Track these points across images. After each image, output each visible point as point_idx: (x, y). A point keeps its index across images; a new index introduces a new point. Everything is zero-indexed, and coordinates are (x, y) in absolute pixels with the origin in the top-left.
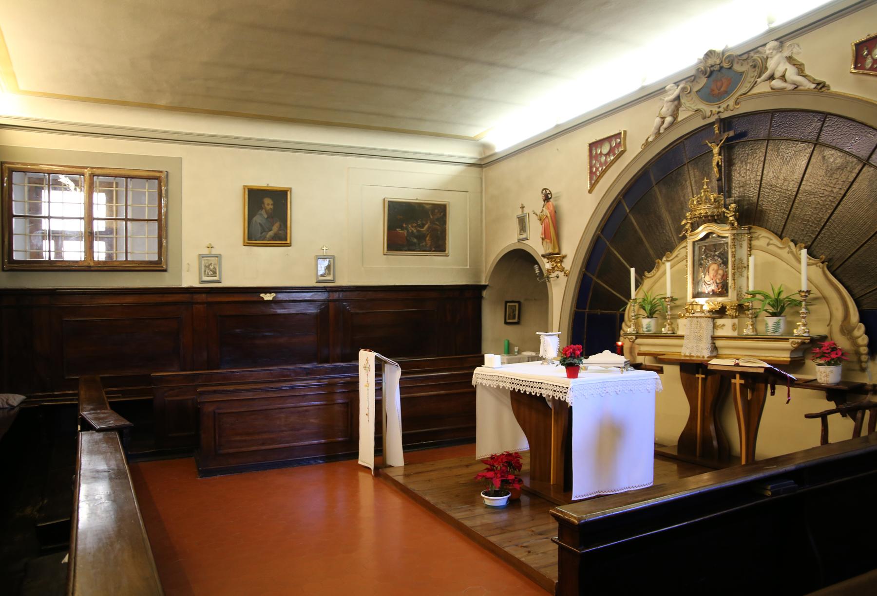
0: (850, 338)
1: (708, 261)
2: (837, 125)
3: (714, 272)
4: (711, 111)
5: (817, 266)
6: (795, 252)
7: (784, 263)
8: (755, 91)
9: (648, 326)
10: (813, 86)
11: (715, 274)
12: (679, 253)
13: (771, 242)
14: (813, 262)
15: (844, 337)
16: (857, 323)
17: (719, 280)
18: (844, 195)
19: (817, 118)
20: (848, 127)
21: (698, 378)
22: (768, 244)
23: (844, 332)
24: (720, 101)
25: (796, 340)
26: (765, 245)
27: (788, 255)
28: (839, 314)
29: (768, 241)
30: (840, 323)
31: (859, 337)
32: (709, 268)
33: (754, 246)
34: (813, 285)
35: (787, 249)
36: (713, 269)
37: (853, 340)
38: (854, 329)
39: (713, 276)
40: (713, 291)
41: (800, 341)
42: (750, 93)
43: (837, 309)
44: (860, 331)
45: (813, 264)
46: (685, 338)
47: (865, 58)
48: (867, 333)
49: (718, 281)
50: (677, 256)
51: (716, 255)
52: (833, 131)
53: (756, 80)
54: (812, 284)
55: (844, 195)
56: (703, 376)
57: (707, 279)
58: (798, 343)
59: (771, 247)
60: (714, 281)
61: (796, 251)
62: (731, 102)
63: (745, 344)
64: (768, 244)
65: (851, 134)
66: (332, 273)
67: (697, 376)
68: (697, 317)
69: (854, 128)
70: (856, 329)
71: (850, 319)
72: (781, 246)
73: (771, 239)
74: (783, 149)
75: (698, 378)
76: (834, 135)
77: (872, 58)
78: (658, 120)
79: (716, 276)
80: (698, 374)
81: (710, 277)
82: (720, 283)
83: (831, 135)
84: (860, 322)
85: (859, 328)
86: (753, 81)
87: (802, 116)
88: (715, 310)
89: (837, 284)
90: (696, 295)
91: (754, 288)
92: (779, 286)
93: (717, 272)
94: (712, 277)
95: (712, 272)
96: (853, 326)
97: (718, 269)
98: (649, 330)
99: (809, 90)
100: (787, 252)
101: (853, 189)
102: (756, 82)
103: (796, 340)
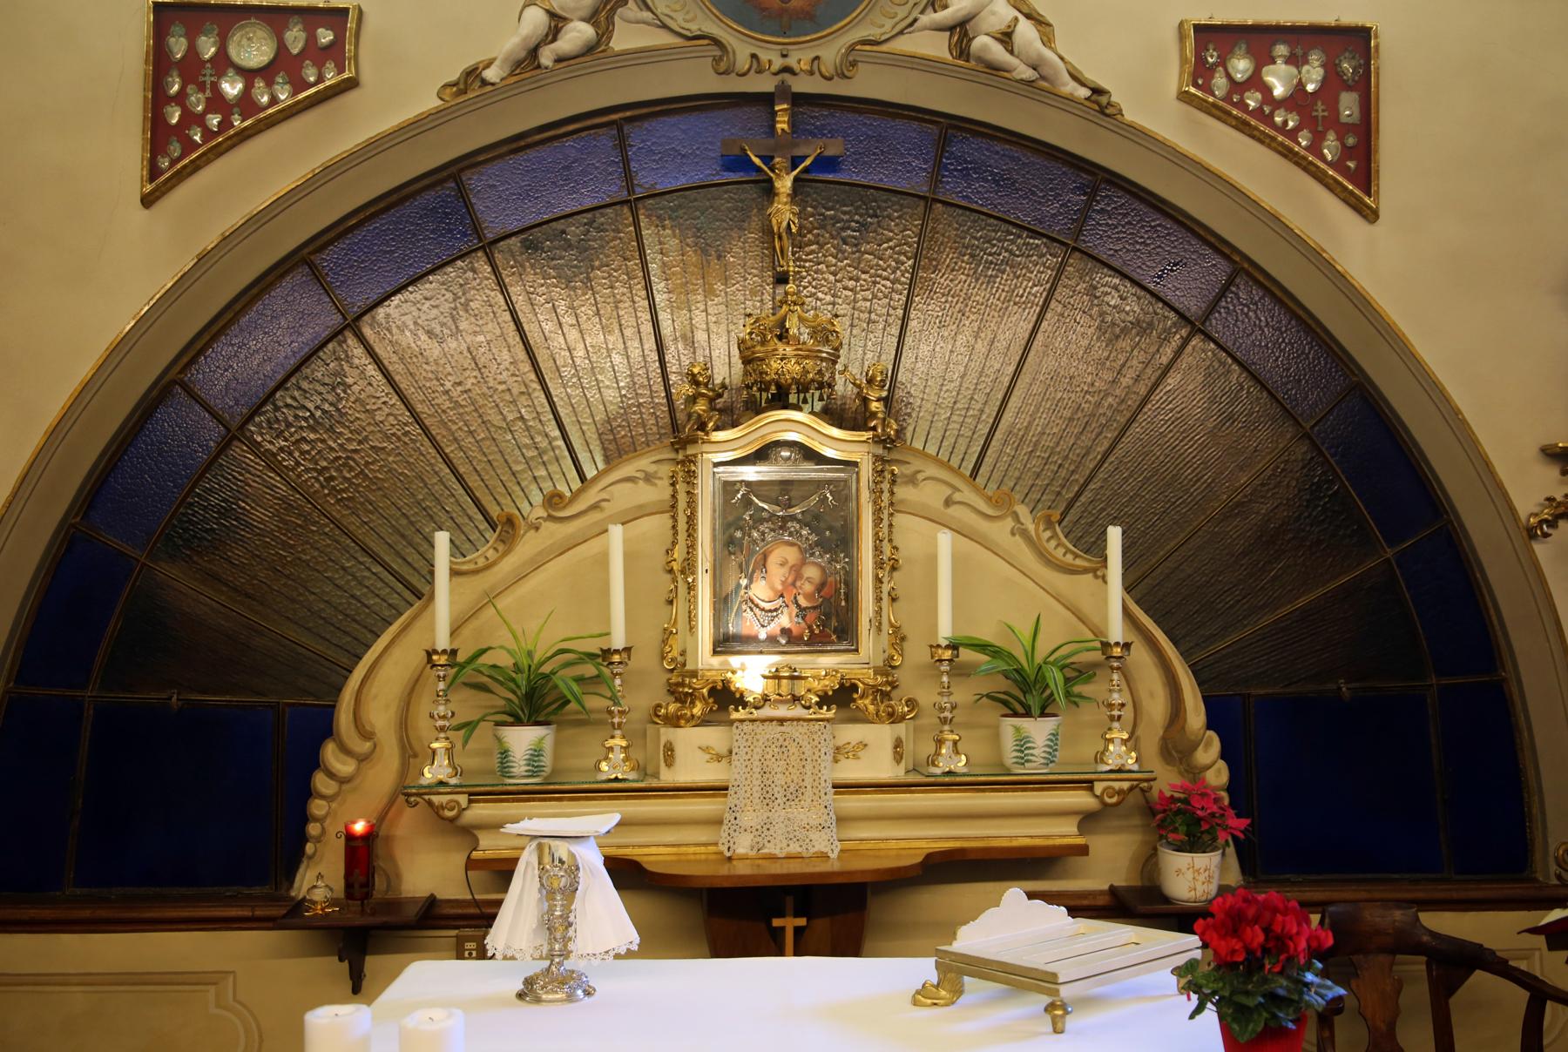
0: (1186, 771)
1: (763, 533)
2: (1125, 215)
3: (785, 570)
4: (754, 56)
5: (1096, 577)
6: (1033, 533)
7: (1001, 560)
8: (904, 45)
9: (536, 754)
10: (1083, 93)
11: (790, 580)
12: (604, 495)
13: (957, 497)
14: (1086, 564)
15: (1170, 768)
16: (1202, 731)
17: (807, 596)
18: (1145, 401)
19: (1074, 182)
20: (1152, 227)
21: (783, 929)
22: (948, 502)
23: (1170, 754)
24: (784, 34)
25: (1117, 785)
26: (937, 503)
27: (1013, 539)
28: (1156, 707)
29: (948, 491)
30: (1161, 733)
31: (1208, 767)
32: (765, 557)
33: (902, 501)
34: (1087, 626)
35: (1009, 523)
36: (779, 560)
37: (1195, 773)
38: (1195, 746)
39: (783, 583)
40: (785, 631)
41: (1126, 785)
42: (884, 48)
43: (1152, 695)
44: (1209, 752)
45: (1085, 571)
46: (730, 792)
47: (1211, 70)
48: (1224, 755)
49: (803, 602)
50: (595, 507)
51: (793, 518)
52: (1116, 227)
53: (915, 14)
54: (1084, 623)
55: (1145, 401)
56: (802, 922)
57: (760, 590)
58: (1120, 792)
59: (954, 511)
60: (788, 598)
61: (1037, 530)
62: (831, 52)
63: (938, 803)
64: (948, 502)
65: (1160, 247)
66: (1097, 171)
67: (776, 922)
68: (781, 721)
69: (1168, 234)
70: (1201, 748)
71: (1185, 720)
72: (990, 512)
73: (957, 489)
74: (975, 238)
75: (783, 929)
76: (1119, 239)
77: (1229, 76)
78: (535, 19)
79: (794, 584)
80: (782, 915)
81: (772, 588)
82: (814, 608)
83: (1110, 237)
84: (1209, 727)
85: (1209, 744)
86: (901, 14)
87: (1034, 163)
88: (834, 691)
89: (1150, 628)
90: (725, 643)
91: (953, 633)
92: (485, 647)
93: (797, 571)
94: (780, 587)
95: (777, 574)
96: (1193, 738)
97: (803, 563)
98: (534, 770)
99: (1070, 99)
100: (1009, 529)
101: (1168, 388)
102: (915, 20)
103: (1117, 785)
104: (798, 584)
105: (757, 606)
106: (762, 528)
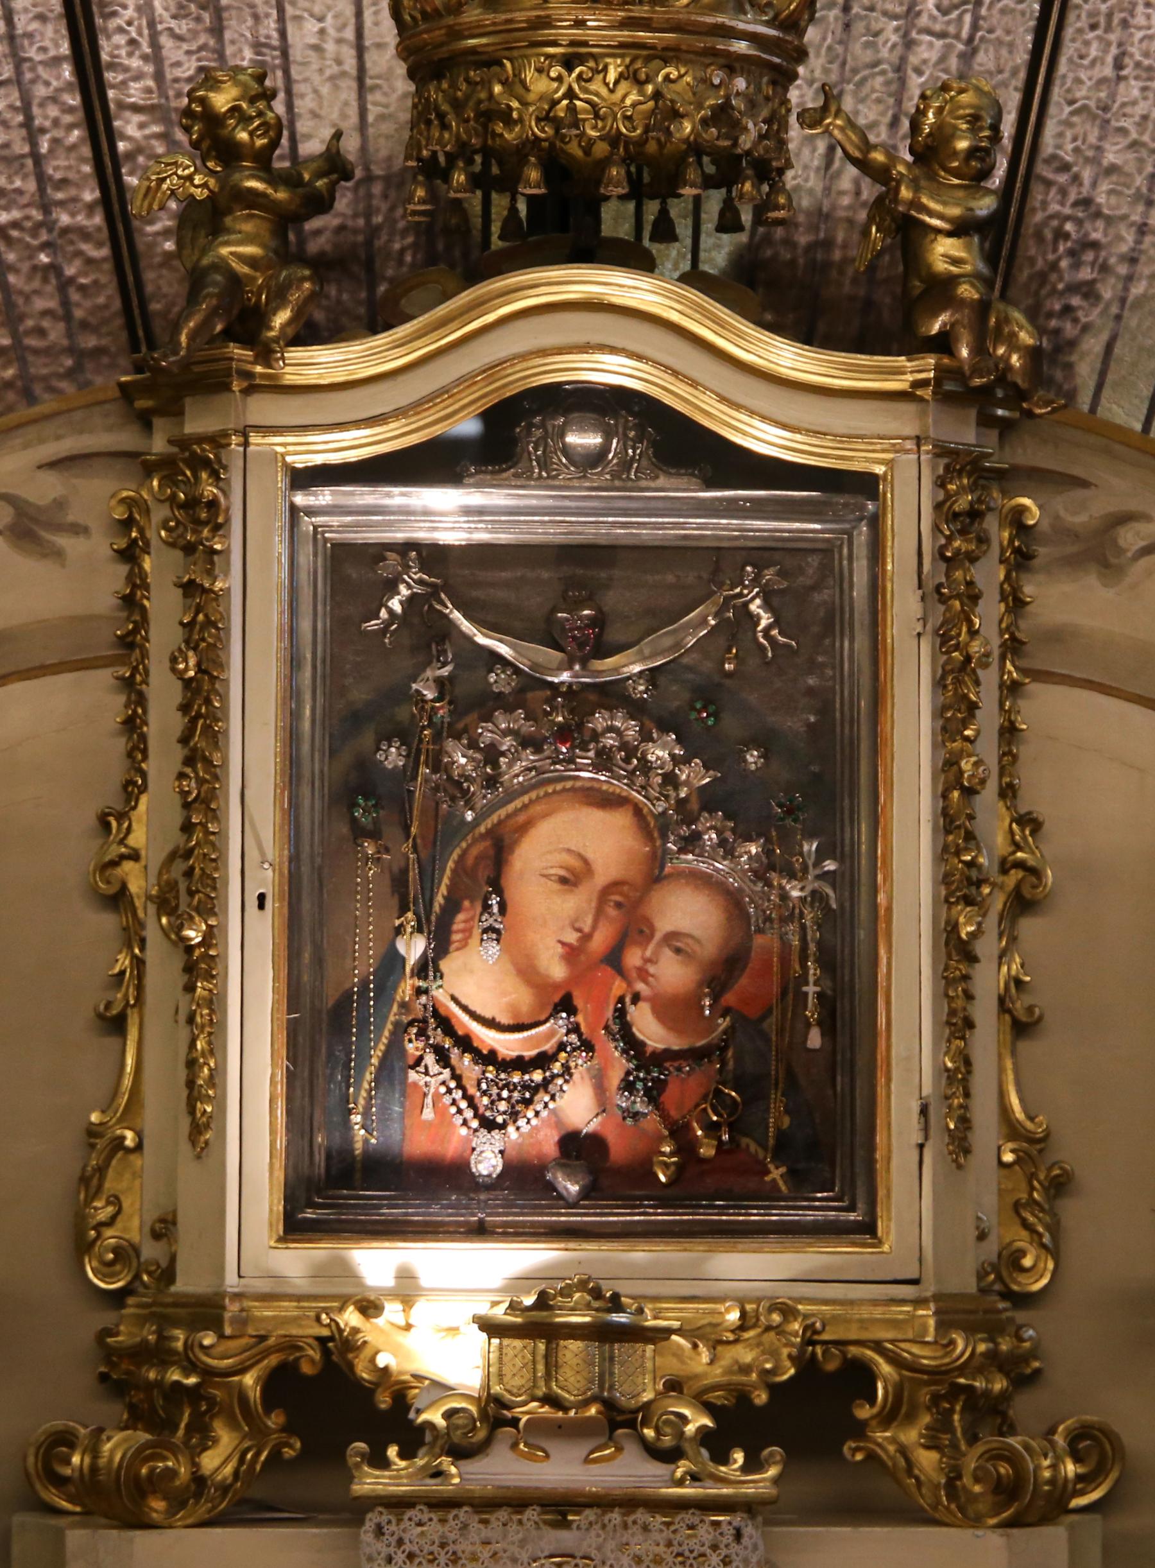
11: (600, 941)
39: (571, 954)
79: (614, 959)
81: (527, 971)
82: (696, 1055)
94: (557, 971)
104: (633, 958)
105: (466, 1043)
106: (486, 734)
